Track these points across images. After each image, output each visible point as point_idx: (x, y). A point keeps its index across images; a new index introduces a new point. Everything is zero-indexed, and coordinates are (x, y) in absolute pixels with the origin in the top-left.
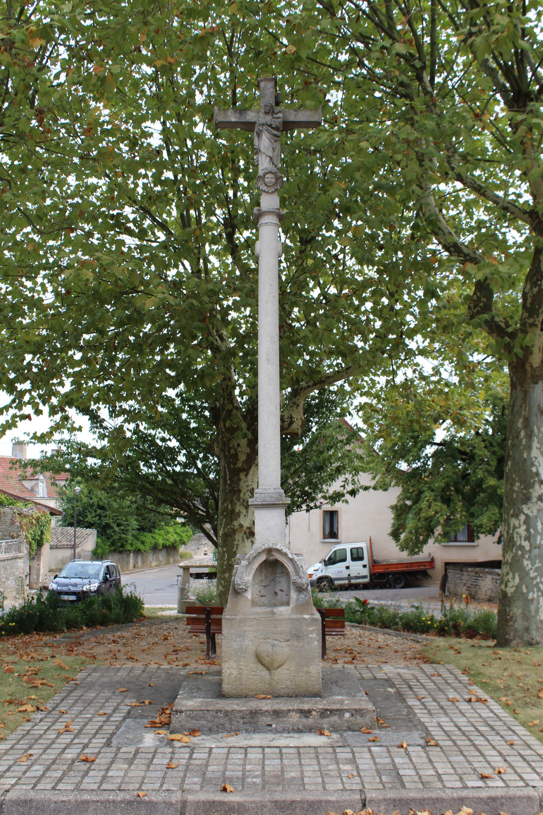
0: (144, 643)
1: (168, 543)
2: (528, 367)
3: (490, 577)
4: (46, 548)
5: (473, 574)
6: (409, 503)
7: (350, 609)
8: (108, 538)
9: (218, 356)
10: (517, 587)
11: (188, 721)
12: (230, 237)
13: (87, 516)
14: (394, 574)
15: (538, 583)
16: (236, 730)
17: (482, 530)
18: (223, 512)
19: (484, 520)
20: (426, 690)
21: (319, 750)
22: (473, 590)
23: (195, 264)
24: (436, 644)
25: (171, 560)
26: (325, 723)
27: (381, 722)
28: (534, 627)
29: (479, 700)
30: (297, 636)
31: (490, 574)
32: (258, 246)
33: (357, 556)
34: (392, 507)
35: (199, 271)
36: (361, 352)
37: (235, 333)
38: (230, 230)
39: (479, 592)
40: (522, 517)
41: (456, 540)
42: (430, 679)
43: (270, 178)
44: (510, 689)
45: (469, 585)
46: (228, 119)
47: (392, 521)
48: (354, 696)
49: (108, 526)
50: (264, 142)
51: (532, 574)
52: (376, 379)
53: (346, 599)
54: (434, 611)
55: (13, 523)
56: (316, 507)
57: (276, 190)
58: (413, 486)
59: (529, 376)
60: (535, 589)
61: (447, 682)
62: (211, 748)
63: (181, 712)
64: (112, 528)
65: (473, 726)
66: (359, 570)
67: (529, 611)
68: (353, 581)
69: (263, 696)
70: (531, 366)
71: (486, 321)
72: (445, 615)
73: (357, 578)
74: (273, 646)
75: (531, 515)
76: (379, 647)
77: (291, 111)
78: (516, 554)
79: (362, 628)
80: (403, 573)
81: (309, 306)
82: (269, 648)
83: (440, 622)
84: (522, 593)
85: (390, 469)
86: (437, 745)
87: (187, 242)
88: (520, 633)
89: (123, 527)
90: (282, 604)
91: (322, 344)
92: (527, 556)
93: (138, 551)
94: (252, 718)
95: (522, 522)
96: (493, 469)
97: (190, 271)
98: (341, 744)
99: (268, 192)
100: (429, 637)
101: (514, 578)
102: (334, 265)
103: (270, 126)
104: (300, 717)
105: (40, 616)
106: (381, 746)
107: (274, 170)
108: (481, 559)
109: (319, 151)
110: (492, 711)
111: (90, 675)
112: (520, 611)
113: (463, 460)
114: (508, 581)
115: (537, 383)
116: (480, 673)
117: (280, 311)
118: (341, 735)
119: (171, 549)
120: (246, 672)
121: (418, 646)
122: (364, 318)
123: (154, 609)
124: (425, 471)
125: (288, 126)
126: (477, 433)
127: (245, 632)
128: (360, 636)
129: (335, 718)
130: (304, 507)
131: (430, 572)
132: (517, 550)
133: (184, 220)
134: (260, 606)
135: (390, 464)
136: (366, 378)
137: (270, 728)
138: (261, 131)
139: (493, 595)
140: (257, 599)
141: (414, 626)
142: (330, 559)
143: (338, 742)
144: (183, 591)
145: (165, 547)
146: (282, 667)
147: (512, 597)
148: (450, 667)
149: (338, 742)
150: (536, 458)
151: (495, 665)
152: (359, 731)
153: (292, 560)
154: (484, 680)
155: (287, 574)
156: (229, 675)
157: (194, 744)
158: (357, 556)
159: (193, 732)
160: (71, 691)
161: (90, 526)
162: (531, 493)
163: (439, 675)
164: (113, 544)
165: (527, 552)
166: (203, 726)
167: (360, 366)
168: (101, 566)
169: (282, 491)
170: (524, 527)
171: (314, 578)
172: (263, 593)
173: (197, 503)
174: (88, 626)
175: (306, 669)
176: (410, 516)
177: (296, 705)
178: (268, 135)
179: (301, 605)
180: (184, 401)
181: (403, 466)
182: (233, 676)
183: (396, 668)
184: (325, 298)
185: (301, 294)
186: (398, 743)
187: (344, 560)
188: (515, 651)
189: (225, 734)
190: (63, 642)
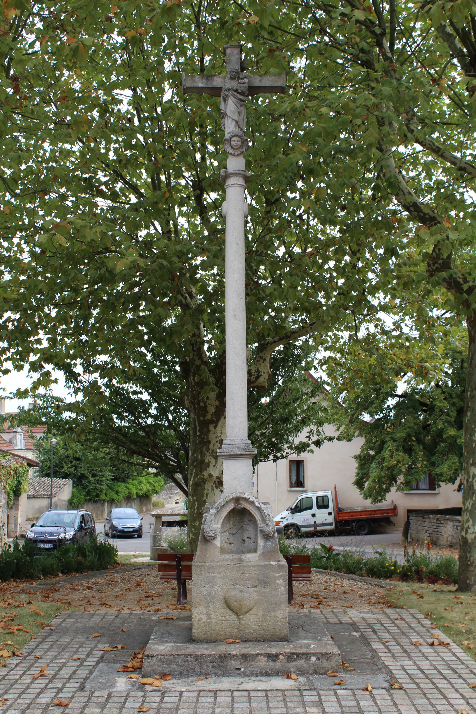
1: (141, 493)
3: (451, 524)
4: (23, 498)
5: (435, 521)
6: (372, 453)
7: (316, 555)
8: (84, 488)
9: (187, 312)
12: (199, 199)
13: (63, 467)
16: (206, 674)
18: (193, 462)
19: (444, 469)
20: (390, 633)
22: (435, 536)
23: (165, 224)
24: (399, 589)
25: (144, 509)
26: (292, 666)
27: (346, 665)
30: (264, 582)
31: (451, 520)
32: (225, 207)
33: (322, 504)
34: (356, 457)
35: (169, 232)
36: (325, 308)
37: (203, 290)
38: (198, 192)
41: (417, 489)
42: (393, 623)
43: (236, 142)
45: (431, 531)
46: (195, 85)
48: (320, 640)
49: (83, 476)
50: (230, 107)
52: (340, 333)
53: (312, 545)
54: (398, 557)
56: (283, 457)
57: (242, 153)
58: (375, 437)
61: (410, 626)
62: (182, 692)
63: (153, 656)
64: (87, 478)
65: (436, 669)
66: (324, 517)
68: (319, 528)
69: (232, 640)
72: (408, 561)
74: (241, 591)
76: (344, 592)
79: (328, 574)
80: (367, 521)
81: (275, 264)
82: (238, 594)
83: (403, 567)
85: (354, 420)
86: (401, 688)
87: (158, 204)
89: (98, 478)
90: (250, 551)
91: (287, 300)
94: (221, 662)
96: (453, 420)
97: (161, 232)
98: (307, 687)
99: (234, 155)
100: (392, 582)
102: (298, 225)
103: (236, 91)
105: (17, 564)
106: (346, 689)
107: (240, 133)
108: (442, 507)
109: (284, 116)
110: (454, 655)
114: (468, 527)
116: (442, 618)
117: (246, 270)
118: (308, 678)
120: (215, 617)
121: (381, 591)
122: (328, 276)
123: (128, 556)
124: (387, 422)
125: (254, 91)
127: (214, 578)
129: (302, 662)
130: (271, 457)
131: (392, 519)
133: (156, 184)
134: (229, 553)
136: (330, 334)
137: (238, 672)
138: (227, 96)
139: (454, 541)
141: (378, 571)
142: (296, 507)
143: (304, 685)
146: (250, 612)
148: (413, 611)
149: (304, 685)
152: (325, 674)
153: (259, 509)
154: (446, 625)
155: (255, 521)
156: (199, 620)
158: (322, 504)
159: (164, 676)
160: (46, 637)
161: (66, 476)
163: (403, 619)
164: (89, 493)
166: (174, 670)
167: (324, 322)
168: (76, 515)
171: (282, 525)
172: (231, 540)
173: (168, 454)
174: (63, 573)
175: (273, 614)
176: (374, 465)
177: (263, 649)
178: (234, 100)
179: (268, 552)
183: (361, 613)
184: (290, 256)
185: (267, 253)
186: (363, 686)
187: (310, 508)
189: (195, 678)
190: (40, 589)
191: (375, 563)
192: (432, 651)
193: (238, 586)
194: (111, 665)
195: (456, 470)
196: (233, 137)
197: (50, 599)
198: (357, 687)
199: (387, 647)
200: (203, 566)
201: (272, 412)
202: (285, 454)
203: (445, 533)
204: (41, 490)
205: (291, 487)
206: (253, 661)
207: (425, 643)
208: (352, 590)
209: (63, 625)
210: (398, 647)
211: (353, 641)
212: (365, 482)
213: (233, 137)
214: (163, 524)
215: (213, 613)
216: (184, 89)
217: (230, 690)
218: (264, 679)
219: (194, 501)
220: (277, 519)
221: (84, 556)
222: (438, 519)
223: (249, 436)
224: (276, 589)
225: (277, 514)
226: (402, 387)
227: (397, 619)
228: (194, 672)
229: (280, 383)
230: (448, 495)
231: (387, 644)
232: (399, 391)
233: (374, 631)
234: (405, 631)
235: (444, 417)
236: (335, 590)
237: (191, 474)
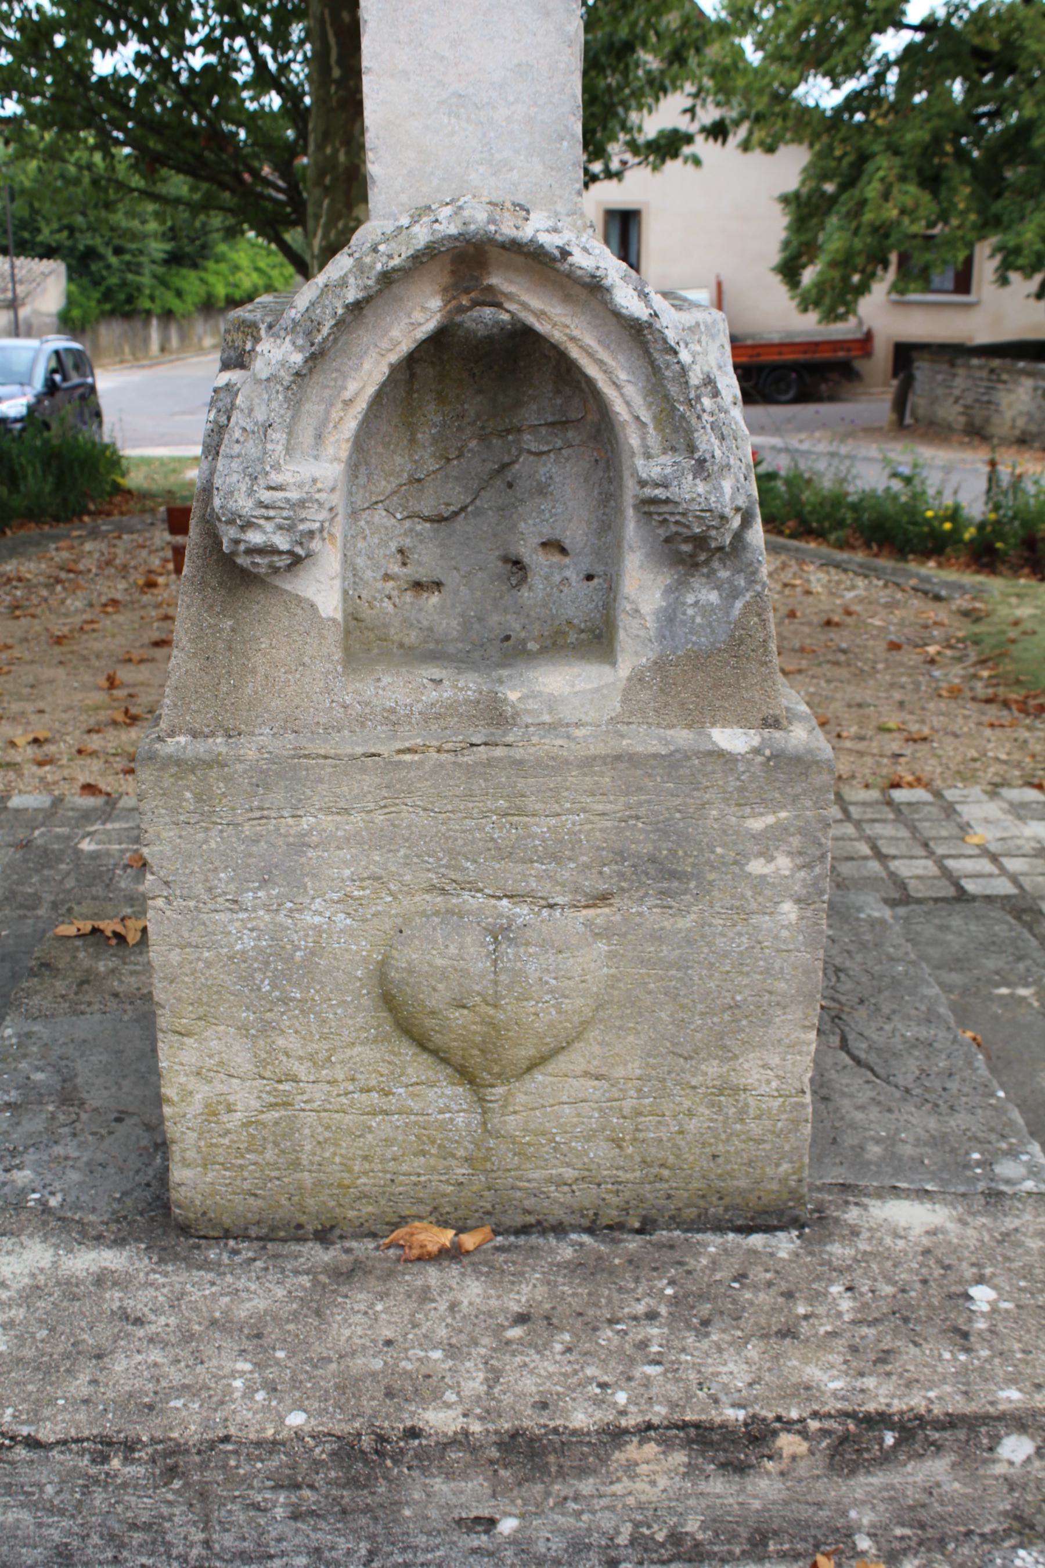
0: (75, 603)
3: (1028, 383)
5: (984, 374)
6: (829, 188)
8: (96, 283)
13: (38, 230)
17: (1021, 261)
22: (979, 415)
30: (664, 869)
31: (1029, 374)
34: (785, 200)
39: (996, 420)
45: (969, 401)
47: (783, 235)
49: (91, 254)
58: (843, 141)
72: (997, 508)
74: (500, 933)
82: (473, 954)
83: (981, 526)
89: (127, 257)
93: (168, 315)
94: (353, 1482)
104: (691, 1471)
108: (983, 337)
120: (318, 1093)
123: (179, 460)
127: (301, 844)
129: (937, 1469)
131: (859, 365)
137: (482, 1540)
139: (1033, 428)
140: (388, 606)
146: (561, 1063)
155: (598, 429)
156: (211, 1112)
161: (48, 253)
164: (111, 299)
168: (38, 351)
172: (427, 561)
175: (712, 1069)
176: (833, 220)
179: (698, 660)
191: (890, 508)
193: (471, 901)
200: (218, 762)
203: (1010, 405)
206: (583, 1471)
212: (804, 267)
215: (302, 1070)
222: (992, 371)
224: (742, 912)
230: (1002, 308)
237: (317, 217)
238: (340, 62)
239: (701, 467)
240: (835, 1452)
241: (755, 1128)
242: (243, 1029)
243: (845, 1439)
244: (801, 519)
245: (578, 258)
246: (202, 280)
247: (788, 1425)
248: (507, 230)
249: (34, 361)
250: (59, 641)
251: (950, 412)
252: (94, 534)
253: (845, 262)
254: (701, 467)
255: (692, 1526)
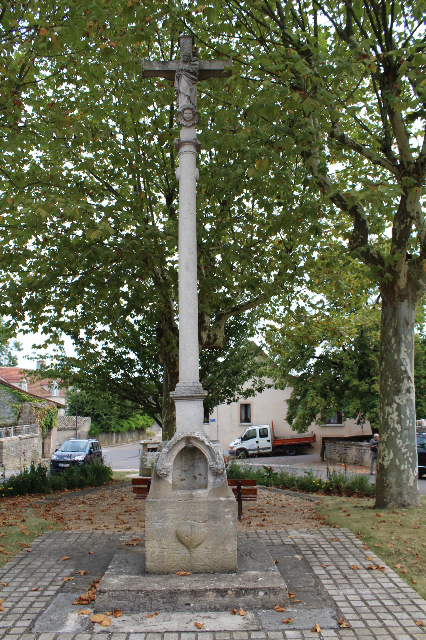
0: (105, 504)
1: (138, 427)
2: (396, 289)
3: (355, 448)
4: (54, 431)
5: (343, 445)
6: (298, 398)
7: (260, 474)
8: (99, 424)
10: (391, 460)
11: (111, 601)
14: (289, 445)
15: (408, 457)
16: (156, 610)
18: (166, 405)
19: (351, 408)
20: (328, 556)
21: (234, 634)
24: (325, 503)
25: (141, 438)
26: (241, 601)
27: (294, 597)
28: (406, 492)
29: (378, 567)
30: (214, 517)
31: (355, 445)
33: (263, 434)
34: (287, 401)
39: (348, 458)
40: (395, 406)
41: (329, 422)
42: (330, 543)
43: (188, 114)
44: (401, 554)
46: (153, 68)
47: (287, 410)
48: (267, 571)
49: (98, 415)
51: (404, 450)
52: (276, 308)
53: (257, 465)
54: (321, 474)
55: (31, 413)
56: (234, 401)
59: (397, 295)
60: (406, 462)
61: (345, 547)
62: (129, 634)
63: (104, 592)
64: (101, 416)
65: (378, 599)
66: (265, 443)
67: (402, 480)
68: (261, 451)
69: (183, 573)
70: (399, 288)
71: (363, 253)
72: (330, 479)
73: (264, 449)
74: (192, 526)
75: (401, 403)
76: (283, 506)
77: (206, 61)
78: (391, 434)
79: (269, 490)
80: (295, 445)
83: (326, 484)
84: (396, 466)
85: (285, 375)
86: (349, 627)
88: (395, 497)
90: (200, 487)
92: (399, 436)
93: (118, 432)
94: (171, 597)
95: (394, 409)
96: (356, 373)
98: (255, 627)
99: (186, 127)
100: (318, 496)
101: (389, 454)
104: (217, 596)
105: (32, 482)
106: (294, 629)
107: (191, 106)
108: (347, 435)
110: (392, 581)
111: (44, 541)
112: (394, 480)
113: (335, 368)
114: (384, 456)
115: (403, 301)
116: (371, 537)
118: (256, 613)
119: (141, 430)
120: (167, 550)
121: (311, 504)
123: (124, 472)
124: (309, 376)
126: (344, 349)
127: (166, 513)
128: (268, 497)
130: (226, 401)
131: (312, 444)
132: (391, 432)
134: (181, 489)
135: (285, 371)
137: (188, 607)
138: (180, 75)
139: (357, 460)
140: (178, 483)
141: (306, 487)
142: (245, 436)
143: (252, 624)
144: (143, 461)
145: (137, 429)
146: (201, 546)
147: (388, 469)
148: (345, 530)
149: (252, 624)
150: (404, 359)
151: (382, 529)
152: (272, 608)
153: (209, 447)
154: (376, 545)
155: (205, 459)
156: (152, 553)
157: (114, 627)
158: (263, 434)
159: (115, 612)
160: (22, 559)
161: (87, 415)
162: (401, 387)
163: (338, 540)
164: (102, 427)
165: (399, 433)
166: (125, 605)
168: (87, 443)
169: (200, 385)
170: (396, 413)
171: (235, 449)
172: (183, 477)
173: (151, 400)
174: (68, 488)
175: (222, 547)
176: (300, 406)
177: (212, 583)
178: (186, 78)
179: (218, 488)
180: (142, 328)
181: (294, 373)
182: (155, 555)
183: (300, 532)
186: (311, 626)
187: (255, 437)
188: (393, 512)
189: (145, 614)
190: (44, 503)
191: (305, 481)
192: (370, 576)
194: (70, 595)
195: (358, 409)
196: (185, 109)
197: (51, 513)
198: (306, 626)
199: (328, 572)
200: (156, 502)
201: (227, 367)
202: (236, 398)
204: (69, 424)
205: (241, 422)
206: (202, 596)
207: (361, 567)
208: (289, 504)
209: (41, 546)
210: (338, 572)
211: (296, 566)
213: (185, 109)
214: (149, 450)
215: (165, 547)
216: (143, 73)
217: (177, 632)
218: (212, 614)
219: (166, 435)
220: (232, 445)
221: (86, 475)
223: (200, 381)
225: (232, 441)
226: (319, 351)
227: (333, 540)
228: (145, 608)
229: (232, 346)
231: (328, 568)
232: (317, 354)
233: (314, 553)
234: (341, 553)
235: (350, 372)
236: (275, 505)
238: (170, 380)
239: (216, 463)
240: (236, 594)
241: (229, 556)
242: (157, 540)
243: (237, 592)
244: (284, 485)
245: (201, 439)
246: (128, 423)
247: (230, 589)
248: (192, 435)
249: (86, 446)
250: (103, 511)
251: (336, 456)
252: (108, 489)
253: (304, 417)
254: (216, 463)
255: (217, 606)
